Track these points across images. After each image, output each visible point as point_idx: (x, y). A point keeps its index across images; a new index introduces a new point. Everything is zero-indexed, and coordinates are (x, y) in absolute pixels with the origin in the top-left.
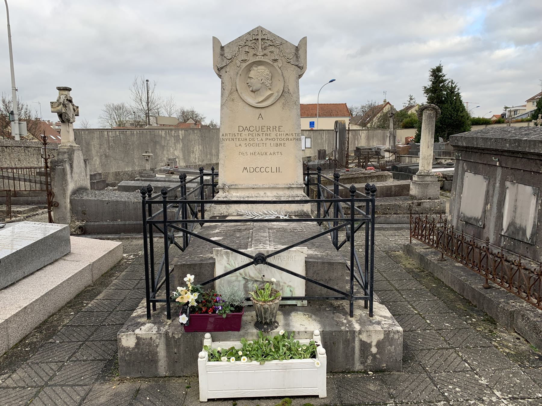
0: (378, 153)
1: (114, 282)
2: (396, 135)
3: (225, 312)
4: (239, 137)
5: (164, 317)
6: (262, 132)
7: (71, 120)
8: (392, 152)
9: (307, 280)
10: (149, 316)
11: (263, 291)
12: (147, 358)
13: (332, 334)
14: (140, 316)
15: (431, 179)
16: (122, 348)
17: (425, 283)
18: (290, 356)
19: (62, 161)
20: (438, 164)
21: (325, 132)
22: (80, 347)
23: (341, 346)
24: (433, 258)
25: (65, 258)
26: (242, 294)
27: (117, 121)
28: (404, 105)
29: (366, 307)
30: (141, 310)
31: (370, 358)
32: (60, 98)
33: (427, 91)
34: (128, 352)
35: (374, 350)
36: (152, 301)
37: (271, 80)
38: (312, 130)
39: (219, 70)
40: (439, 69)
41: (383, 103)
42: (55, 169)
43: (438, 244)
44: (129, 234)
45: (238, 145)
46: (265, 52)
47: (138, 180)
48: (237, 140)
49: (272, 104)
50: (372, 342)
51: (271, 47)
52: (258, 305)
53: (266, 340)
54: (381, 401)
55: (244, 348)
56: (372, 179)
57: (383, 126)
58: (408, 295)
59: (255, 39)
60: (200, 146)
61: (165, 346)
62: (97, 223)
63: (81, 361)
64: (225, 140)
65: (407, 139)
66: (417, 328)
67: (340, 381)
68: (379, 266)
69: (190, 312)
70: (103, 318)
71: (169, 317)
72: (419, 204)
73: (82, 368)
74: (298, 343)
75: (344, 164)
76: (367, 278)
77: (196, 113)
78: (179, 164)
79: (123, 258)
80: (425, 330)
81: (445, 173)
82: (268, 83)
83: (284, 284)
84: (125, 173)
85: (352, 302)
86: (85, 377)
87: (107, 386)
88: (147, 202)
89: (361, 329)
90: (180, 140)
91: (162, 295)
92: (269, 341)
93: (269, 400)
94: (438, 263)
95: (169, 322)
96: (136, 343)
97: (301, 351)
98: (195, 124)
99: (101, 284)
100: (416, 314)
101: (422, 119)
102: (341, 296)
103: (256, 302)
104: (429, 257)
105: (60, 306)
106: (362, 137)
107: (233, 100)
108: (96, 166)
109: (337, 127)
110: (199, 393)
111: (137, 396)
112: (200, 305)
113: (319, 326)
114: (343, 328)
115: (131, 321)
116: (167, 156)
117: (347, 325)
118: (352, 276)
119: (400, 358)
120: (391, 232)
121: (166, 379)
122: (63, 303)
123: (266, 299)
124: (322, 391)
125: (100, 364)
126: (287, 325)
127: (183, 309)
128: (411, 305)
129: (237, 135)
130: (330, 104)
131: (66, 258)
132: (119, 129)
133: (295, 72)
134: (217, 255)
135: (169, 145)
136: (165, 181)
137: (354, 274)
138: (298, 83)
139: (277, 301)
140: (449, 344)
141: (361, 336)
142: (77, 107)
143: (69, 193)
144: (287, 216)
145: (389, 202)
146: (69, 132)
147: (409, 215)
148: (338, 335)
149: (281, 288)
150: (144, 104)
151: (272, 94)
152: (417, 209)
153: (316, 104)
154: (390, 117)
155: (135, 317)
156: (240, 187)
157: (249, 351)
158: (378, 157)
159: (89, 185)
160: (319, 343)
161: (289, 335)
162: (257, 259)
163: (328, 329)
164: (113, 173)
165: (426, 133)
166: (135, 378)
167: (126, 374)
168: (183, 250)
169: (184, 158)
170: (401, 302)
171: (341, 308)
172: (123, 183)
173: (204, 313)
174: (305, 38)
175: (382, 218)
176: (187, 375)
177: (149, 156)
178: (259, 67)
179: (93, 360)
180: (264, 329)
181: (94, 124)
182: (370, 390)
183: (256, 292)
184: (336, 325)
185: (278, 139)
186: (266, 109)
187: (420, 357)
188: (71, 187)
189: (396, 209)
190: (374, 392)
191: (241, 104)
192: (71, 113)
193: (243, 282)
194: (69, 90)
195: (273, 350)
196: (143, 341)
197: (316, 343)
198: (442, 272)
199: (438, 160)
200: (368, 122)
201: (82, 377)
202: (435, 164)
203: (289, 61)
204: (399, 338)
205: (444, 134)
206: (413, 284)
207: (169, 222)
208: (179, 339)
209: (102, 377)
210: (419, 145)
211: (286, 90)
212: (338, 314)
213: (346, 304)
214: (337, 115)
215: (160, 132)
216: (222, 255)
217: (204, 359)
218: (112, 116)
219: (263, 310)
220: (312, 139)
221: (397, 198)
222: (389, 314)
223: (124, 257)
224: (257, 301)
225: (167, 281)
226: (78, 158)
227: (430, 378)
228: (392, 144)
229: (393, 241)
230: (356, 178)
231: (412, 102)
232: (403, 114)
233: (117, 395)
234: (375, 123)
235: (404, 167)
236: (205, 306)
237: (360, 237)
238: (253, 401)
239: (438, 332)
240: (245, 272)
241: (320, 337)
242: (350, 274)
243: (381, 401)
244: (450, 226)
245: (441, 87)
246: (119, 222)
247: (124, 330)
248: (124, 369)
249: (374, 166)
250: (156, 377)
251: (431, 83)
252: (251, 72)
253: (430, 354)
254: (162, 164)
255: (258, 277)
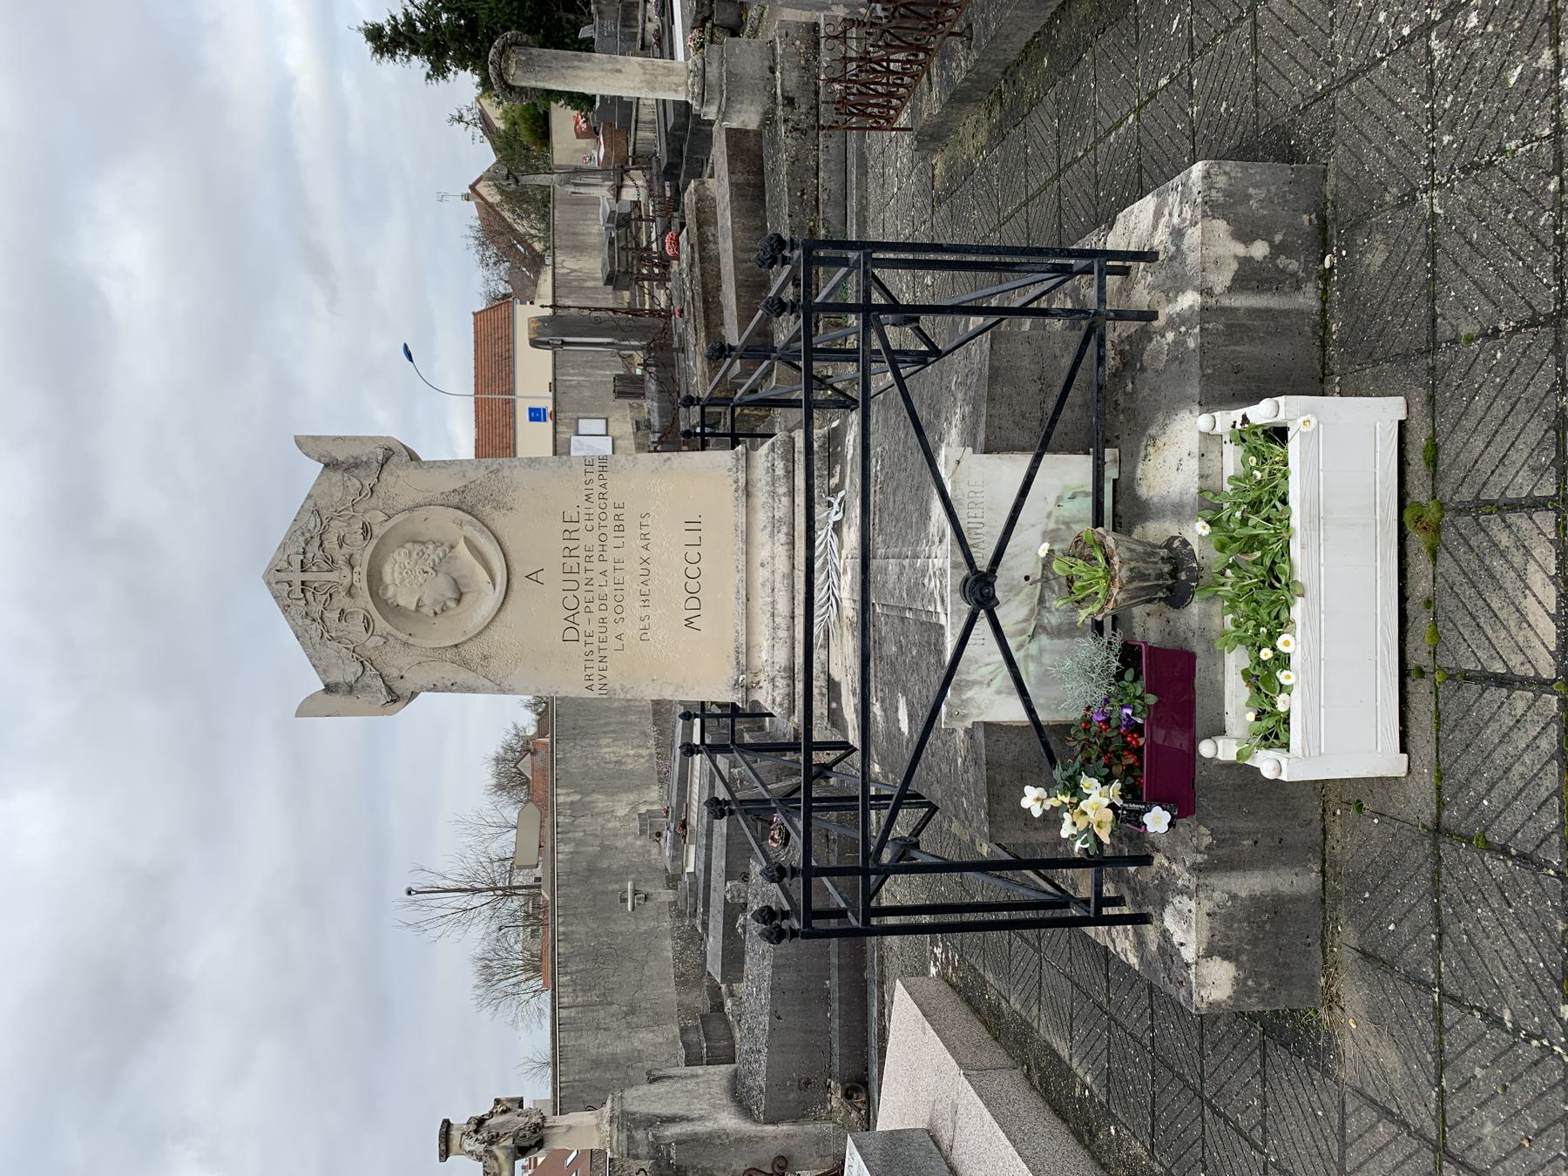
0: (623, 222)
1: (1018, 1007)
2: (568, 166)
3: (1139, 697)
4: (595, 640)
5: (1146, 875)
6: (582, 571)
7: (536, 1119)
8: (622, 180)
9: (1043, 446)
10: (1140, 919)
11: (1077, 584)
12: (1268, 927)
13: (1208, 377)
14: (1141, 944)
15: (715, 65)
16: (1237, 1000)
17: (1038, 89)
18: (1279, 505)
19: (656, 1146)
20: (659, 41)
21: (559, 378)
22: (1220, 1115)
23: (1244, 349)
24: (962, 63)
25: (944, 1147)
26: (1086, 646)
27: (523, 977)
28: (477, 138)
29: (1125, 272)
30: (1121, 942)
31: (1282, 261)
32: (471, 1153)
33: (439, 70)
34: (1250, 983)
35: (1259, 250)
36: (1098, 910)
37: (423, 543)
38: (557, 415)
39: (395, 698)
40: (374, 34)
41: (472, 203)
42: (678, 1168)
43: (919, 48)
44: (869, 959)
45: (620, 643)
46: (341, 561)
47: (705, 925)
48: (602, 645)
49: (498, 541)
50: (1236, 257)
51: (326, 543)
52: (1119, 598)
53: (1223, 575)
54: (1423, 231)
55: (1249, 642)
56: (709, 241)
57: (542, 204)
58: (1075, 142)
59: (303, 590)
60: (603, 742)
61: (1234, 874)
62: (836, 1046)
63: (1264, 1115)
64: (604, 681)
65: (580, 135)
66: (1183, 117)
67: (1353, 354)
68: (979, 227)
69: (1137, 800)
70: (1131, 1044)
71: (1146, 860)
72: (790, 101)
73: (1287, 1112)
74: (1237, 479)
75: (660, 323)
76: (1038, 268)
77: (501, 751)
78: (652, 803)
79: (942, 976)
80: (1190, 91)
81: (689, 22)
82: (433, 554)
83: (1053, 519)
84: (679, 957)
85: (1112, 314)
86: (1315, 1106)
87: (1347, 1045)
88: (807, 924)
89: (1195, 289)
90: (587, 799)
91: (1082, 883)
92: (1230, 566)
93: (1410, 569)
94: (978, 48)
95: (1159, 859)
96: (1224, 959)
97: (1262, 471)
98: (534, 753)
99: (1021, 1044)
100: (1138, 119)
101: (534, 89)
102: (1092, 348)
103: (1111, 605)
104: (959, 77)
105: (1090, 1164)
106: (576, 267)
107: (485, 658)
108: (660, 1040)
109: (548, 343)
110: (1380, 778)
111: (1381, 959)
112: (1117, 770)
113: (1185, 414)
114: (1191, 343)
115: (1155, 971)
116: (630, 839)
117: (1183, 329)
118: (1023, 311)
119: (1287, 171)
120: (871, 187)
121: (1330, 871)
122: (1081, 1155)
123: (1101, 574)
124: (1384, 413)
125: (1277, 1061)
126: (1178, 511)
127: (1130, 822)
128: (1110, 133)
129: (589, 648)
130: (476, 359)
131: (945, 1144)
132: (553, 974)
133: (400, 473)
134: (965, 716)
135: (599, 833)
136: (709, 848)
137: (1016, 304)
138: (433, 464)
139: (1110, 541)
140: (1240, 19)
141: (1218, 290)
142: (498, 1101)
143: (748, 1128)
144: (832, 499)
145: (782, 190)
146: (570, 1128)
147: (821, 133)
148: (1214, 358)
149: (1063, 527)
150: (477, 900)
151: (468, 541)
152: (803, 109)
153: (476, 403)
154: (517, 181)
155: (1142, 959)
156: (743, 639)
157: (1258, 626)
158: (636, 219)
159: (723, 1068)
160: (1237, 415)
161: (1208, 505)
162: (980, 600)
163: (1194, 389)
164: (679, 994)
165: (576, 76)
166: (1325, 962)
167: (1312, 988)
168: (933, 809)
169: (637, 788)
170: (1096, 163)
171: (1127, 348)
172: (714, 967)
173: (1140, 759)
174: (299, 442)
175: (829, 212)
176: (1320, 810)
177: (635, 893)
178: (387, 578)
179: (1264, 1081)
180: (1190, 579)
181: (537, 1039)
182: (1383, 265)
183: (1078, 602)
184: (1181, 363)
185: (603, 523)
186: (513, 556)
187: (1281, 109)
188: (729, 1121)
189: (805, 172)
190: (1390, 252)
191: (495, 634)
192: (516, 1121)
193: (1044, 639)
194: (447, 1125)
195: (1258, 554)
196: (1217, 938)
197: (1238, 426)
198: (1007, 37)
199: (647, 42)
200: (529, 247)
201: (1316, 1115)
202: (662, 51)
203: (367, 490)
204: (1225, 173)
205: (568, 21)
206: (1040, 126)
207: (865, 859)
208: (1213, 832)
209: (1317, 1057)
210: (602, 97)
211: (455, 499)
212: (1145, 357)
213: (1116, 332)
214: (509, 340)
215: (560, 857)
216: (964, 703)
217: (1284, 763)
218: (510, 990)
219: (1136, 584)
220: (581, 415)
221: (768, 166)
222: (1149, 203)
223: (938, 974)
224: (1109, 601)
225: (1036, 865)
226: (645, 1100)
227: (1350, 80)
228: (597, 179)
229: (900, 182)
230: (703, 288)
231: (468, 117)
232: (504, 144)
233: (1375, 1017)
234: (532, 227)
235: (668, 144)
236: (1119, 758)
237: (904, 286)
238: (1411, 619)
239: (1200, 52)
240: (1014, 635)
241: (1217, 414)
242: (1015, 319)
243: (1423, 231)
244: (863, 10)
245: (427, 28)
246: (833, 983)
247: (1183, 992)
248: (1296, 992)
249: (664, 233)
250: (1323, 901)
251: (414, 57)
252: (401, 603)
253: (1271, 77)
254: (655, 851)
255: (1030, 596)
